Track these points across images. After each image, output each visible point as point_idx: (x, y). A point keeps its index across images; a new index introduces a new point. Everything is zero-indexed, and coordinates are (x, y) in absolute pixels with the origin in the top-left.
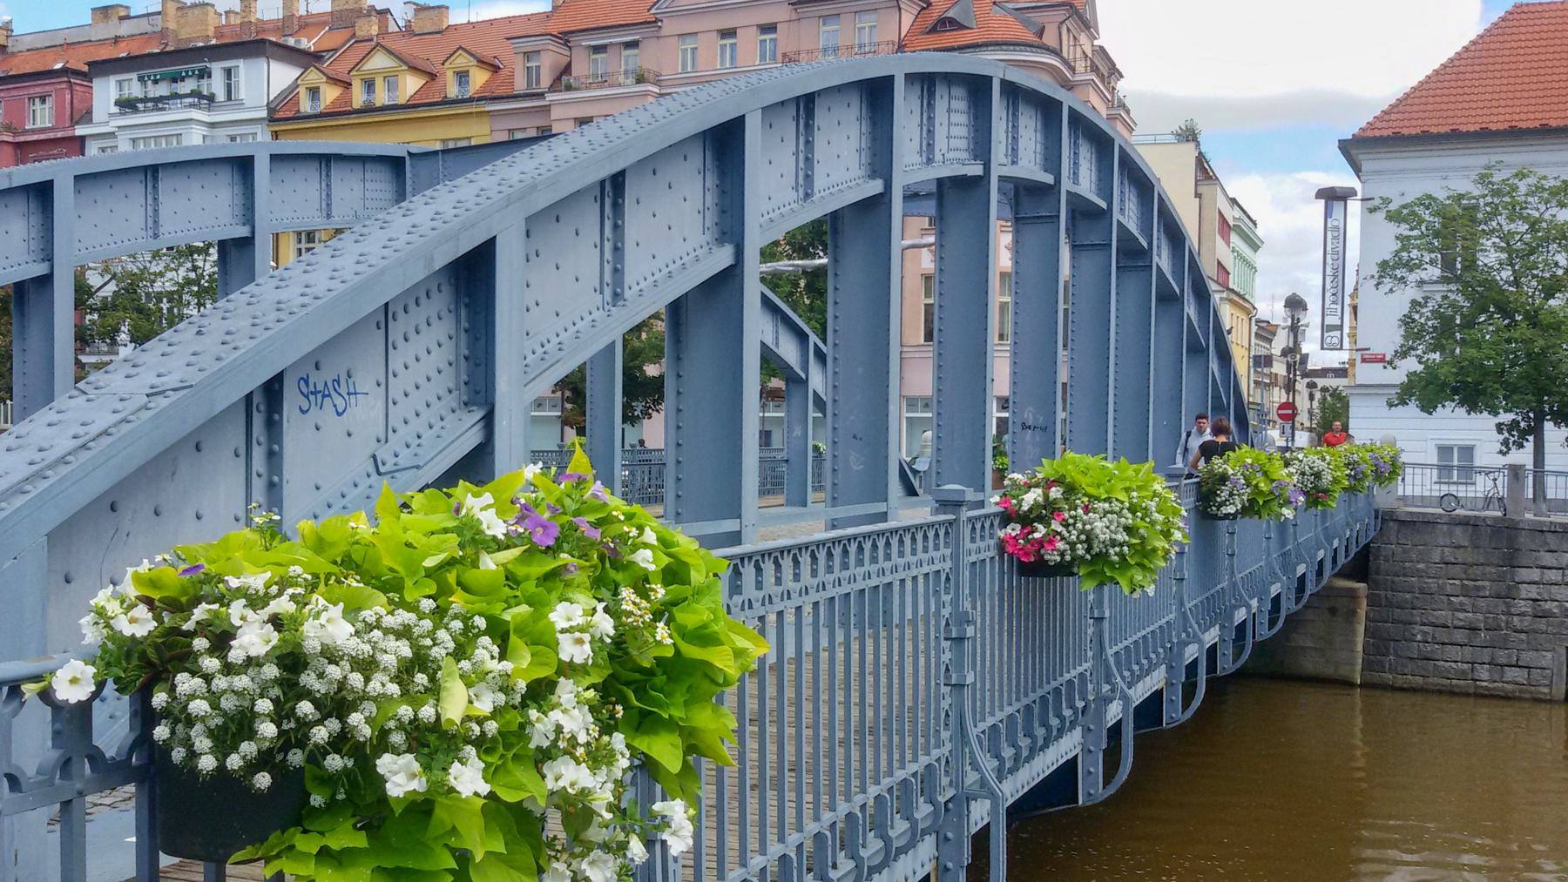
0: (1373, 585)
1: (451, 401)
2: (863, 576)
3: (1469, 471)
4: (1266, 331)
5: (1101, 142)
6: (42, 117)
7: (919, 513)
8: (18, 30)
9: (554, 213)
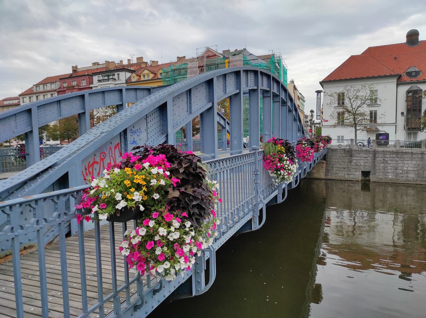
0: (327, 161)
1: (160, 133)
2: (238, 163)
3: (343, 140)
4: (306, 117)
5: (278, 82)
6: (84, 84)
7: (246, 152)
8: (78, 67)
9: (178, 96)
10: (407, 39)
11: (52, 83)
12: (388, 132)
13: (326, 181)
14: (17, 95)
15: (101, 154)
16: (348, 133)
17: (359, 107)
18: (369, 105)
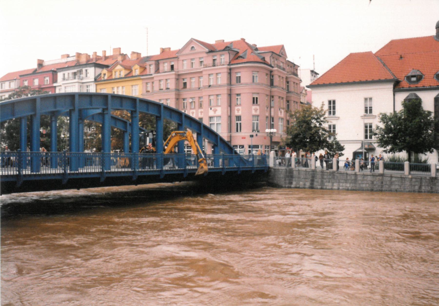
10: (437, 30)
11: (10, 81)
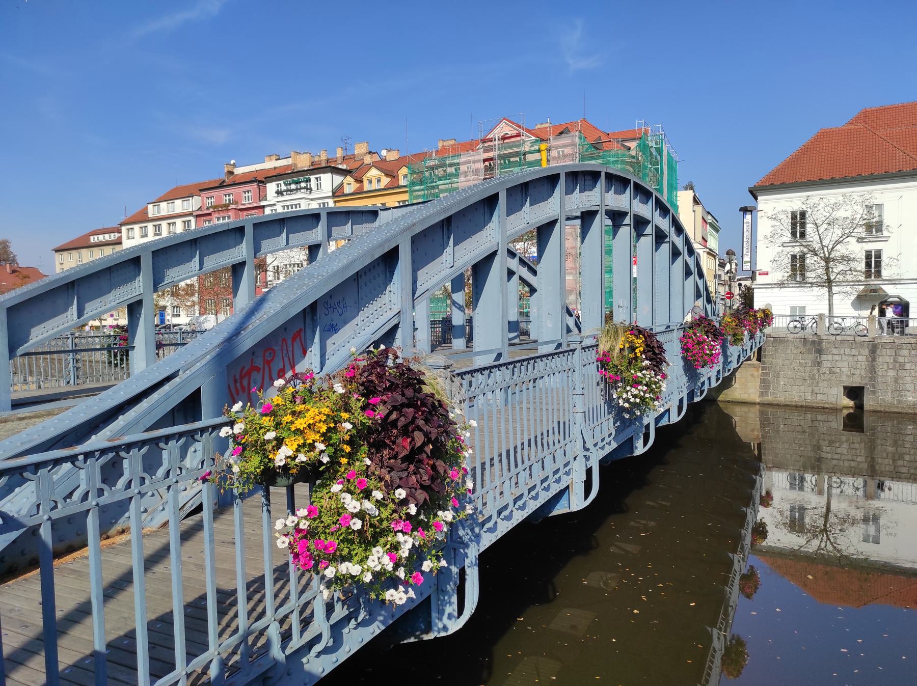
12: (906, 297)
13: (765, 409)
14: (114, 224)
15: (265, 351)
16: (812, 301)
17: (838, 242)
18: (860, 240)
